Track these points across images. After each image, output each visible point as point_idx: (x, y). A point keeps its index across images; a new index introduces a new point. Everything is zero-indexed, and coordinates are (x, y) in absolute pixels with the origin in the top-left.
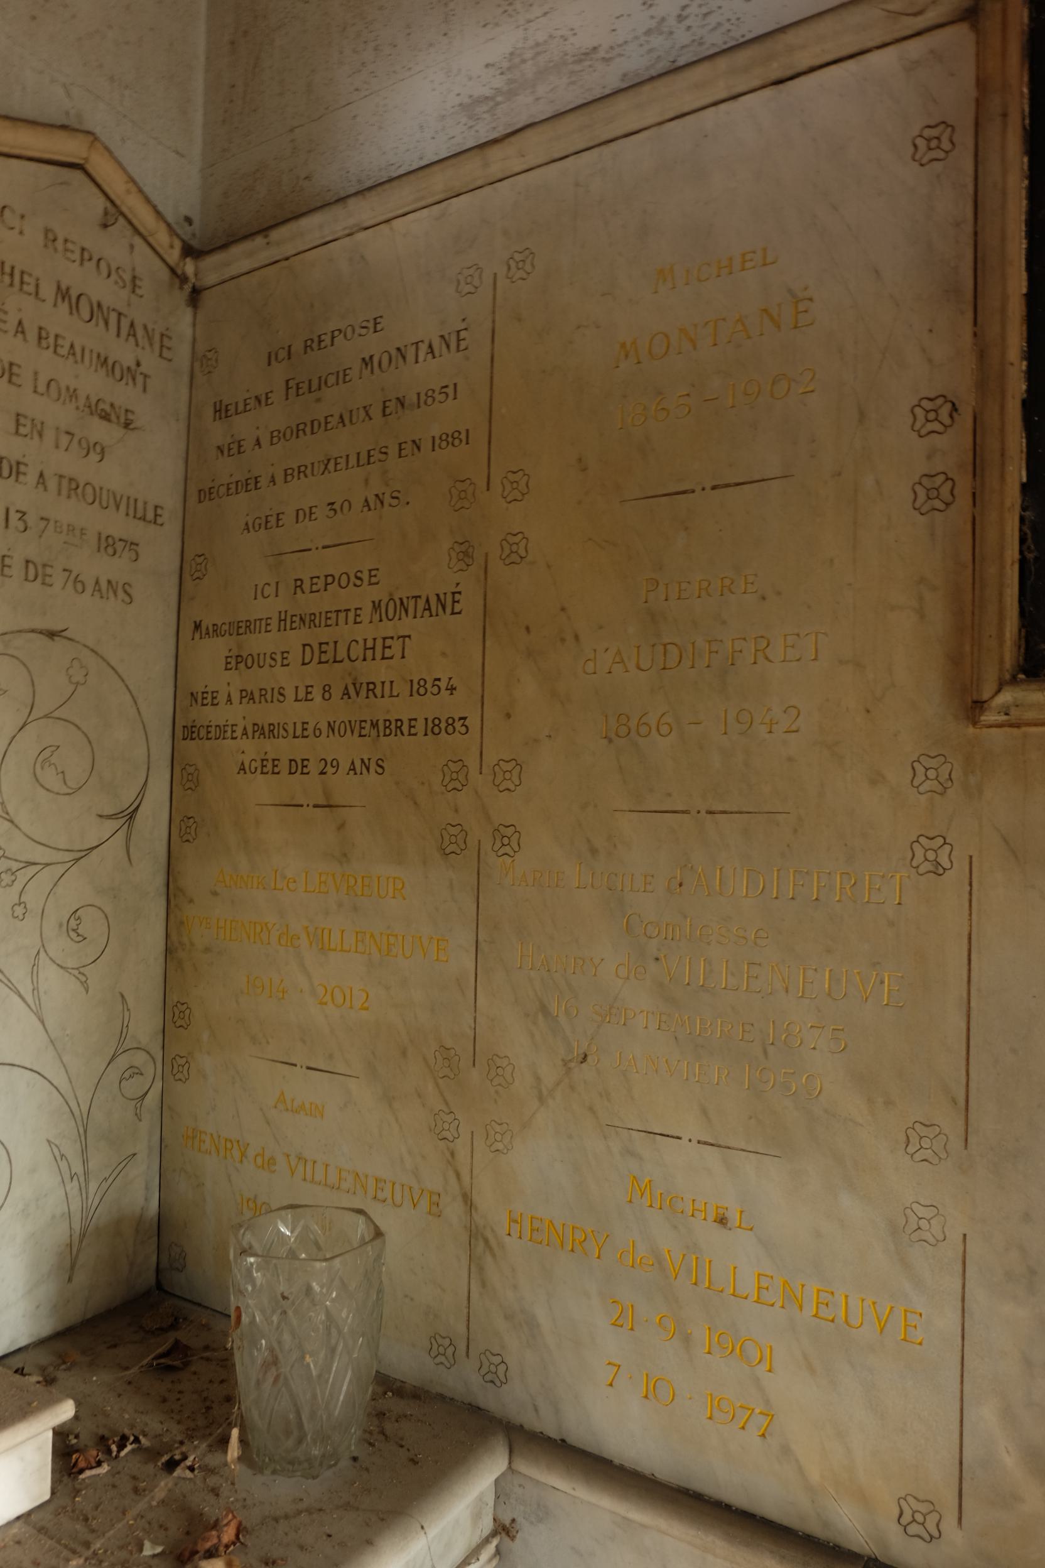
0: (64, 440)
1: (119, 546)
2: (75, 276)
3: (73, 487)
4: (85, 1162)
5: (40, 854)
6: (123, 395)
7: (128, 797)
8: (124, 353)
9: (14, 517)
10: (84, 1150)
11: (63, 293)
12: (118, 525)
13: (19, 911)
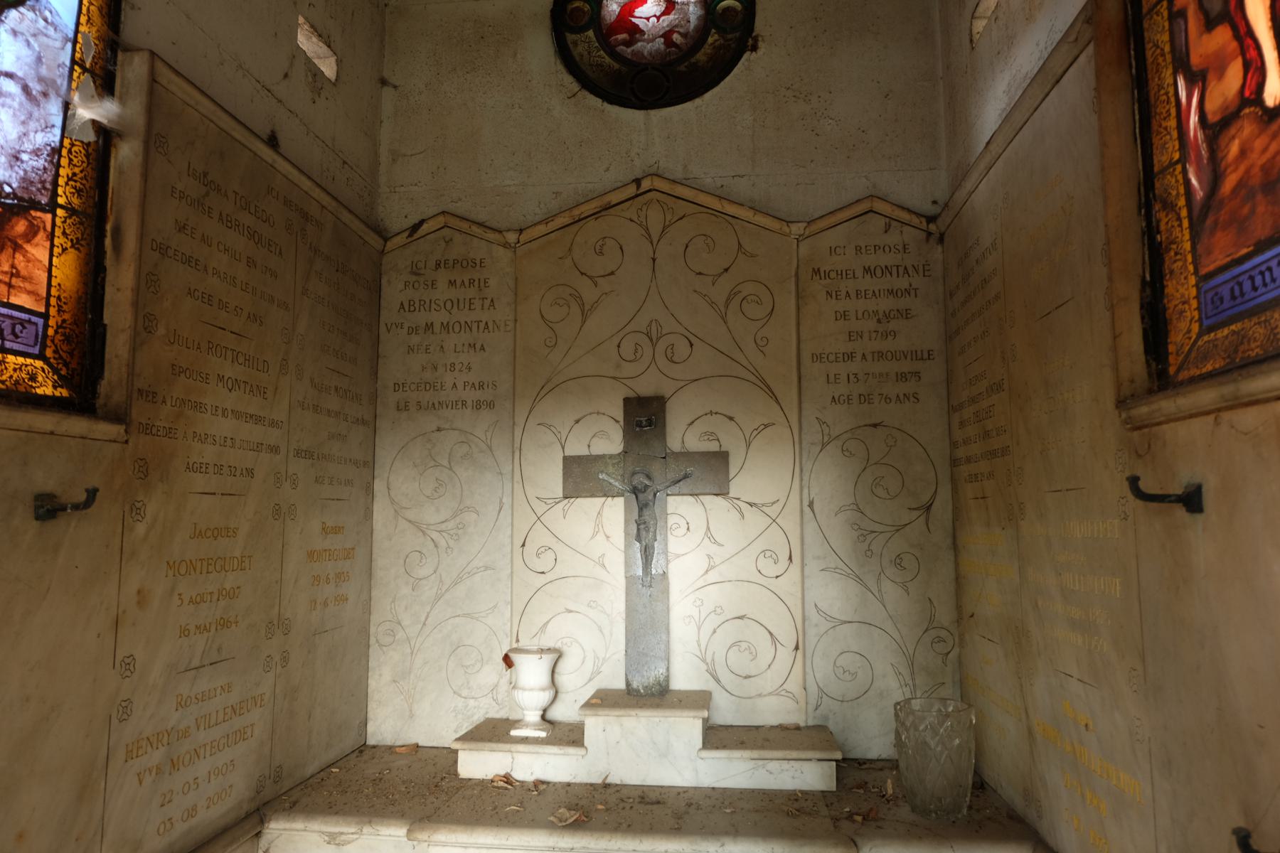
0: (874, 335)
1: (908, 376)
2: (871, 260)
3: (880, 355)
4: (913, 679)
5: (881, 528)
6: (903, 303)
7: (925, 498)
8: (903, 283)
9: (852, 377)
10: (912, 673)
11: (867, 270)
12: (906, 366)
13: (869, 553)
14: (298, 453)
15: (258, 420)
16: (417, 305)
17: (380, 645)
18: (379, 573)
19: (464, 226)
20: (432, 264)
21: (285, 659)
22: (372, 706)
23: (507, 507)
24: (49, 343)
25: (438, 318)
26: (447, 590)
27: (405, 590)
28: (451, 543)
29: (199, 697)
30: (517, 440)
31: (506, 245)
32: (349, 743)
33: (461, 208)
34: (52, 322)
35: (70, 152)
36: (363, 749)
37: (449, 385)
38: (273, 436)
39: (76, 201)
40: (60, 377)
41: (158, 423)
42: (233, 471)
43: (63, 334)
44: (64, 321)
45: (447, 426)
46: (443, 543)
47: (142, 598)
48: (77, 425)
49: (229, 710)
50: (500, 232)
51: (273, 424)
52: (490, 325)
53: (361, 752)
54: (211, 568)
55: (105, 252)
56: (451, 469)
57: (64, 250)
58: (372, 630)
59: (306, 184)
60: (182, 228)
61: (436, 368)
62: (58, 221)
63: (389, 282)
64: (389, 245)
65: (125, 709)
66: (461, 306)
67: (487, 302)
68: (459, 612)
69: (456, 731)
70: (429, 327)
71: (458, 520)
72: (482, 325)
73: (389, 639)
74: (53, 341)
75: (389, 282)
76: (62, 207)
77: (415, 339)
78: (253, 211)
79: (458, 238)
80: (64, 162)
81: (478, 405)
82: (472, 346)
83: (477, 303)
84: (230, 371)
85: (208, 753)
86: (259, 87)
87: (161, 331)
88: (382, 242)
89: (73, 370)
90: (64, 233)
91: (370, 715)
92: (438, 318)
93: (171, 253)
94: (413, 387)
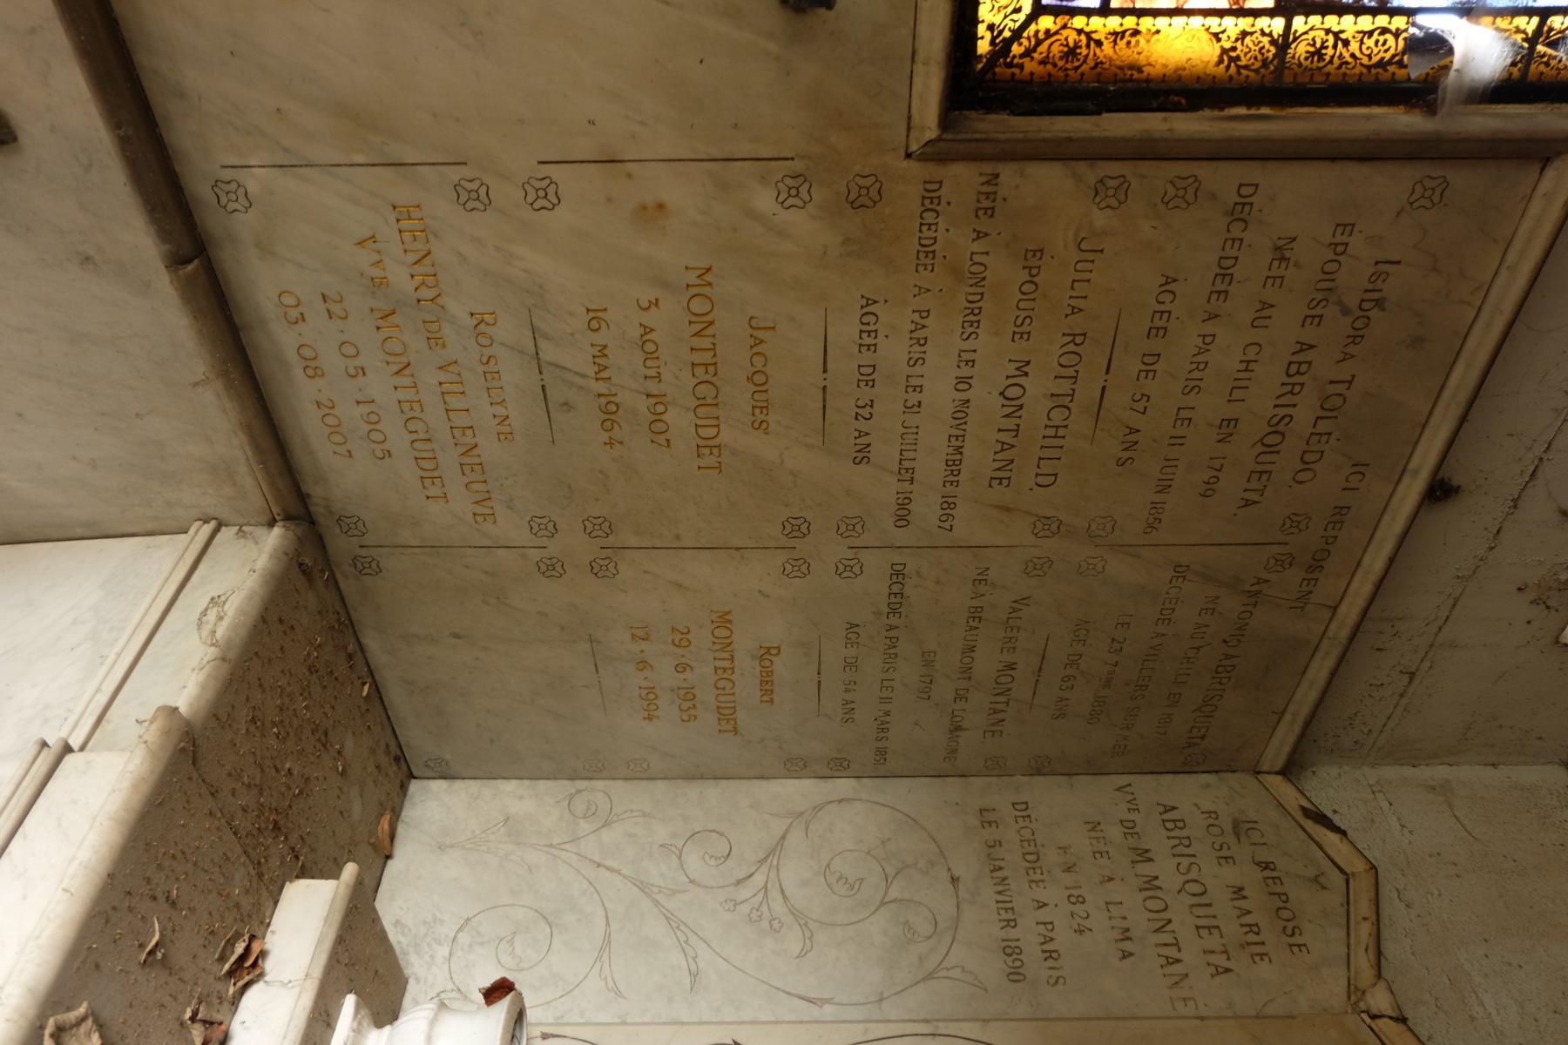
14: (898, 574)
15: (953, 467)
16: (1176, 833)
17: (571, 797)
18: (693, 790)
19: (1363, 907)
20: (1264, 855)
21: (551, 569)
22: (473, 786)
23: (815, 1012)
24: (1061, 20)
25: (1165, 868)
26: (657, 903)
27: (662, 833)
28: (745, 909)
29: (492, 367)
30: (952, 1028)
31: (1354, 991)
32: (415, 737)
33: (1392, 907)
34: (1096, 23)
35: (1384, 31)
36: (402, 769)
37: (1041, 894)
38: (926, 509)
39: (1301, 49)
40: (1007, 43)
41: (942, 226)
42: (864, 411)
43: (1077, 45)
44: (1099, 43)
45: (963, 893)
46: (744, 893)
47: (652, 214)
48: (930, 85)
49: (469, 440)
50: (1379, 976)
51: (948, 505)
52: (1176, 968)
53: (397, 759)
54: (700, 371)
55: (1222, 109)
56: (883, 904)
57: (1217, 36)
58: (599, 784)
59: (1375, 561)
60: (1281, 254)
61: (1068, 870)
62: (1263, 22)
63: (1208, 786)
64: (1276, 782)
65: (473, 197)
66: (1201, 911)
67: (1221, 961)
68: (614, 926)
69: (397, 923)
70: (1144, 856)
71: (789, 919)
72: (1172, 952)
73: (579, 807)
74: (1065, 26)
75: (1208, 786)
76: (1288, 26)
77: (1115, 833)
78: (1323, 426)
79: (1334, 899)
80: (1365, 22)
81: (1011, 950)
82: (1126, 935)
83: (1214, 942)
84: (1037, 387)
85: (401, 394)
86: (1539, 450)
87: (1100, 219)
88: (1280, 763)
89: (1021, 67)
90: (1244, 34)
91: (459, 784)
92: (1165, 868)
93: (1236, 230)
94: (1027, 833)
